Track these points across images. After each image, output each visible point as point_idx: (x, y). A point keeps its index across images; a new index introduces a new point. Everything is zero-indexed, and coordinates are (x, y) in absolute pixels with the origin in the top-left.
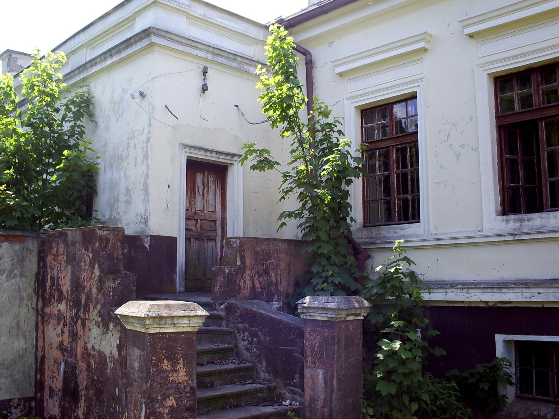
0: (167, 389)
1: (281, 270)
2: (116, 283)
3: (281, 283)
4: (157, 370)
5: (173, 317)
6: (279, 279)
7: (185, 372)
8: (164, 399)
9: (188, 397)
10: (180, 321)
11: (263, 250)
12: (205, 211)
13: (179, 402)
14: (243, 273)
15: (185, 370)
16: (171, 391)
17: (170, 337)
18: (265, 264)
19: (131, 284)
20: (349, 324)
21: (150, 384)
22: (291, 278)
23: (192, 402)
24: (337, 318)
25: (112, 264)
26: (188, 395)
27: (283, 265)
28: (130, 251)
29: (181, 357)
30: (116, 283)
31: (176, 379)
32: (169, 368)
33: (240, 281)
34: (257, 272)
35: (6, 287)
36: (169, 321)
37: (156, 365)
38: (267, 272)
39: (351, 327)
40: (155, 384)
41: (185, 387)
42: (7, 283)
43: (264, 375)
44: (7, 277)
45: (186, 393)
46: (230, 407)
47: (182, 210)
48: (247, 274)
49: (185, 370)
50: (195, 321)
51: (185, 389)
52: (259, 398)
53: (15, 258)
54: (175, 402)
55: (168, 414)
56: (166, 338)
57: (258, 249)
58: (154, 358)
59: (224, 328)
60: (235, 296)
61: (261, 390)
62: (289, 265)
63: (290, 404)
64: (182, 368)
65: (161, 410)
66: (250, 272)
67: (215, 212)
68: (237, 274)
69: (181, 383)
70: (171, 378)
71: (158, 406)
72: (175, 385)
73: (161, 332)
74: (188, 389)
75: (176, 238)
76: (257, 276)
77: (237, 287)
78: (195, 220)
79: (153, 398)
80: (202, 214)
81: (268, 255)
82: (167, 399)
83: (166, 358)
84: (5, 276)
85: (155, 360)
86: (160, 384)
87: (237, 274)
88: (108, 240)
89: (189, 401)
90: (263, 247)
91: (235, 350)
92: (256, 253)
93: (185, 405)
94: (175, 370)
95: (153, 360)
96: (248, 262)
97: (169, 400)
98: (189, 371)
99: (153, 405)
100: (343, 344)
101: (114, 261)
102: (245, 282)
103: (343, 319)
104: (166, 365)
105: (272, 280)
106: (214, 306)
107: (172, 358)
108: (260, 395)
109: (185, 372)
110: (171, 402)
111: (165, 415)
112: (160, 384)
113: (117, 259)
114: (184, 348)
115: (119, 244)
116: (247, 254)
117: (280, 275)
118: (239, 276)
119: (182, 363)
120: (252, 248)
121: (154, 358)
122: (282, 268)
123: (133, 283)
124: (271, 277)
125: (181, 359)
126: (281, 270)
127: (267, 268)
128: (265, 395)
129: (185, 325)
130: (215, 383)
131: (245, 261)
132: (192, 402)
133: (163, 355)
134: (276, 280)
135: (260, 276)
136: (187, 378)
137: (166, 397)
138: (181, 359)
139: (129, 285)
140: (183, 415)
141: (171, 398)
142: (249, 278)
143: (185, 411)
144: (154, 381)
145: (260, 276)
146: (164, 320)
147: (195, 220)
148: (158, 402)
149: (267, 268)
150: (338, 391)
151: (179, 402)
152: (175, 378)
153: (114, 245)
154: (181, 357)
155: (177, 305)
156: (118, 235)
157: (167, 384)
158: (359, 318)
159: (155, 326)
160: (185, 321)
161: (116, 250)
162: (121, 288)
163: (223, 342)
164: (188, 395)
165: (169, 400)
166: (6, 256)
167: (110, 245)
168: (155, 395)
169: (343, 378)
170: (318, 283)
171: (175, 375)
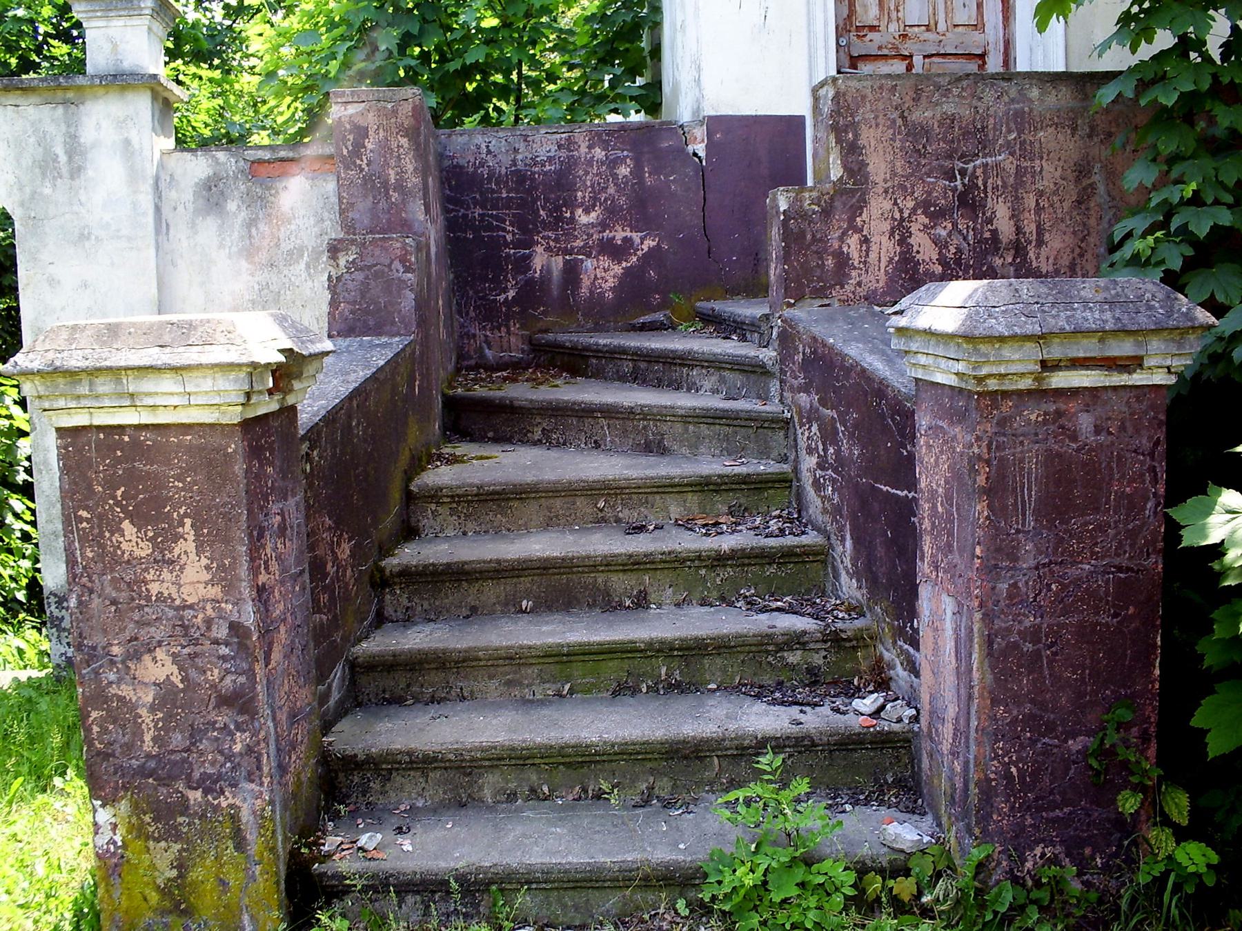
0: (141, 624)
1: (1040, 194)
2: (342, 262)
3: (1040, 243)
4: (101, 557)
5: (115, 372)
6: (1030, 228)
7: (208, 568)
8: (136, 656)
9: (224, 658)
10: (147, 385)
11: (949, 121)
12: (942, 27)
13: (193, 673)
14: (859, 207)
15: (204, 561)
16: (158, 632)
17: (136, 444)
18: (963, 173)
19: (397, 265)
20: (1073, 406)
21: (80, 603)
22: (1092, 222)
23: (242, 679)
24: (980, 380)
25: (383, 204)
26: (224, 650)
27: (1050, 173)
28: (637, 171)
29: (186, 515)
30: (342, 262)
31: (173, 590)
32: (144, 550)
33: (841, 239)
34: (925, 205)
35: (308, 292)
36: (104, 386)
37: (96, 540)
38: (970, 202)
39: (1085, 422)
40: (96, 602)
41: (209, 622)
42: (310, 283)
43: (850, 587)
44: (308, 266)
45: (216, 642)
46: (653, 690)
47: (819, 27)
48: (876, 213)
49: (204, 561)
50: (207, 384)
51: (209, 628)
52: (793, 668)
53: (326, 215)
54: (175, 669)
55: (153, 709)
56: (120, 445)
57: (922, 115)
58: (84, 514)
59: (773, 407)
60: (820, 293)
61: (796, 640)
62: (1082, 170)
63: (876, 714)
64: (193, 556)
65: (126, 691)
66: (887, 205)
67: (979, 26)
68: (827, 213)
69: (191, 607)
70: (154, 588)
71: (112, 677)
72: (171, 613)
73: (96, 422)
74: (221, 632)
75: (804, 117)
76: (923, 219)
77: (830, 262)
78: (904, 57)
79: (94, 648)
80: (930, 36)
81: (978, 137)
82: (147, 658)
83: (130, 516)
84: (302, 266)
85: (88, 520)
86: (114, 602)
87: (827, 213)
88: (361, 133)
89: (228, 672)
90: (949, 108)
91: (795, 483)
92: (918, 133)
93: (214, 686)
94: (164, 561)
95: (80, 520)
96: (878, 166)
97: (155, 660)
98: (222, 567)
99: (97, 673)
100: (1032, 495)
101: (388, 197)
102: (866, 241)
103: (1026, 384)
104: (132, 541)
105: (995, 232)
106: (764, 327)
107: (149, 513)
108: (794, 658)
109: (208, 568)
110: (160, 668)
111: (143, 712)
112: (114, 602)
113: (400, 187)
114: (195, 483)
115: (404, 141)
116: (868, 137)
117: (1039, 209)
118: (839, 220)
119: (191, 537)
120: (895, 115)
121: (84, 514)
122: (1046, 183)
123: (403, 260)
124: (990, 221)
125: (188, 521)
126: (1040, 194)
127: (971, 187)
128: (817, 660)
129: (175, 401)
130: (653, 597)
131: (863, 165)
132: (242, 679)
133: (118, 504)
134: (1019, 230)
135: (937, 215)
136: (215, 592)
137: (139, 650)
138: (188, 521)
139: (390, 266)
140: (212, 716)
141: (160, 654)
142: (886, 226)
143: (217, 706)
144: (91, 591)
145: (937, 215)
146: (86, 382)
147: (904, 57)
148: (113, 663)
149: (971, 187)
150: (995, 702)
151: (193, 673)
152: (167, 589)
153: (384, 146)
154: (186, 515)
155: (598, 329)
156: (395, 112)
157: (140, 608)
158: (1138, 378)
159: (61, 403)
160: (168, 384)
161: (393, 163)
162: (359, 276)
163: (764, 454)
164: (224, 650)
165: (155, 660)
166: (302, 212)
167: (370, 146)
168: (98, 640)
169: (1028, 647)
170: (1129, 235)
171: (166, 575)
